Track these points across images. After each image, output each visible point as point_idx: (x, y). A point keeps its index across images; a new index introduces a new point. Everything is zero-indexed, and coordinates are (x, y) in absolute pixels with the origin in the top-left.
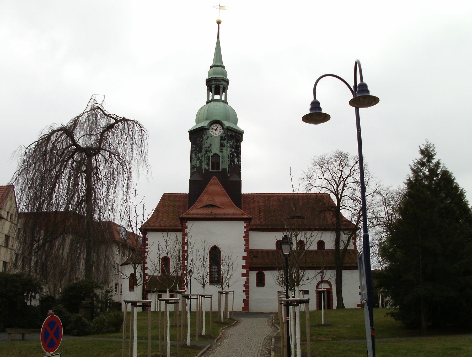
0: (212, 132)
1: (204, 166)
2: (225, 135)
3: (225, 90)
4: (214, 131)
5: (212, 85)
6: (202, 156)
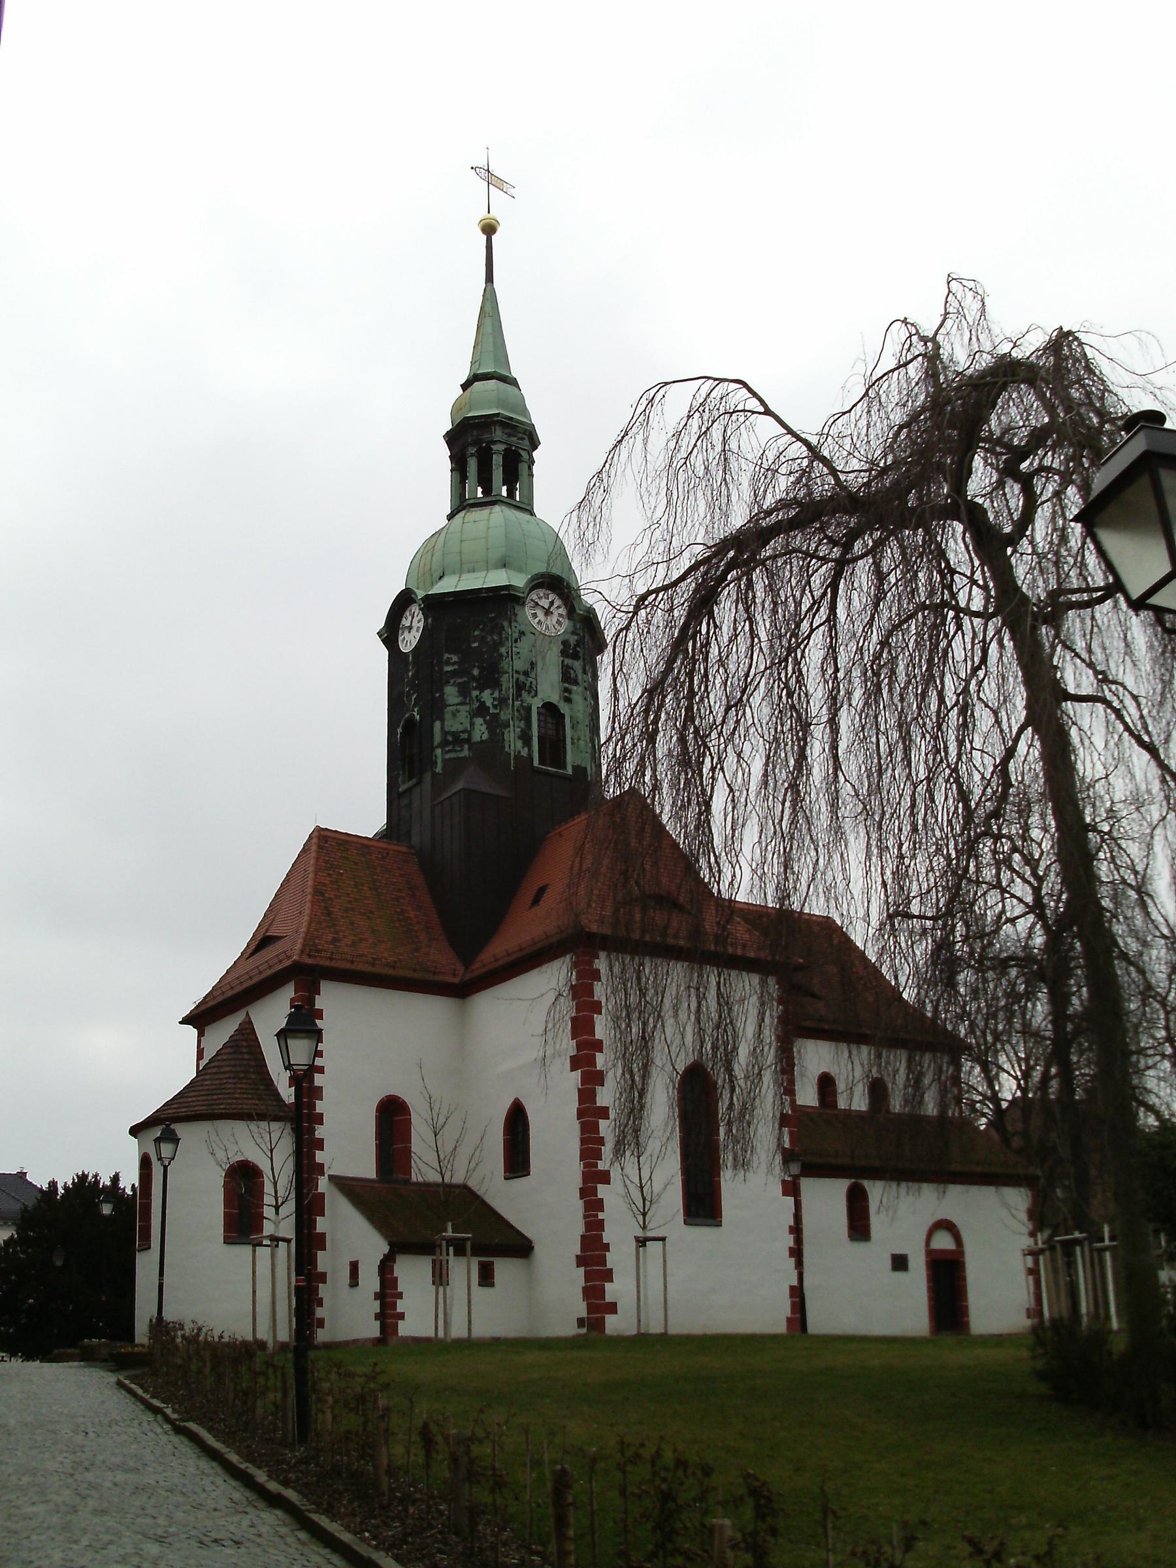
0: (535, 616)
1: (513, 743)
4: (541, 615)
5: (495, 442)
6: (502, 702)
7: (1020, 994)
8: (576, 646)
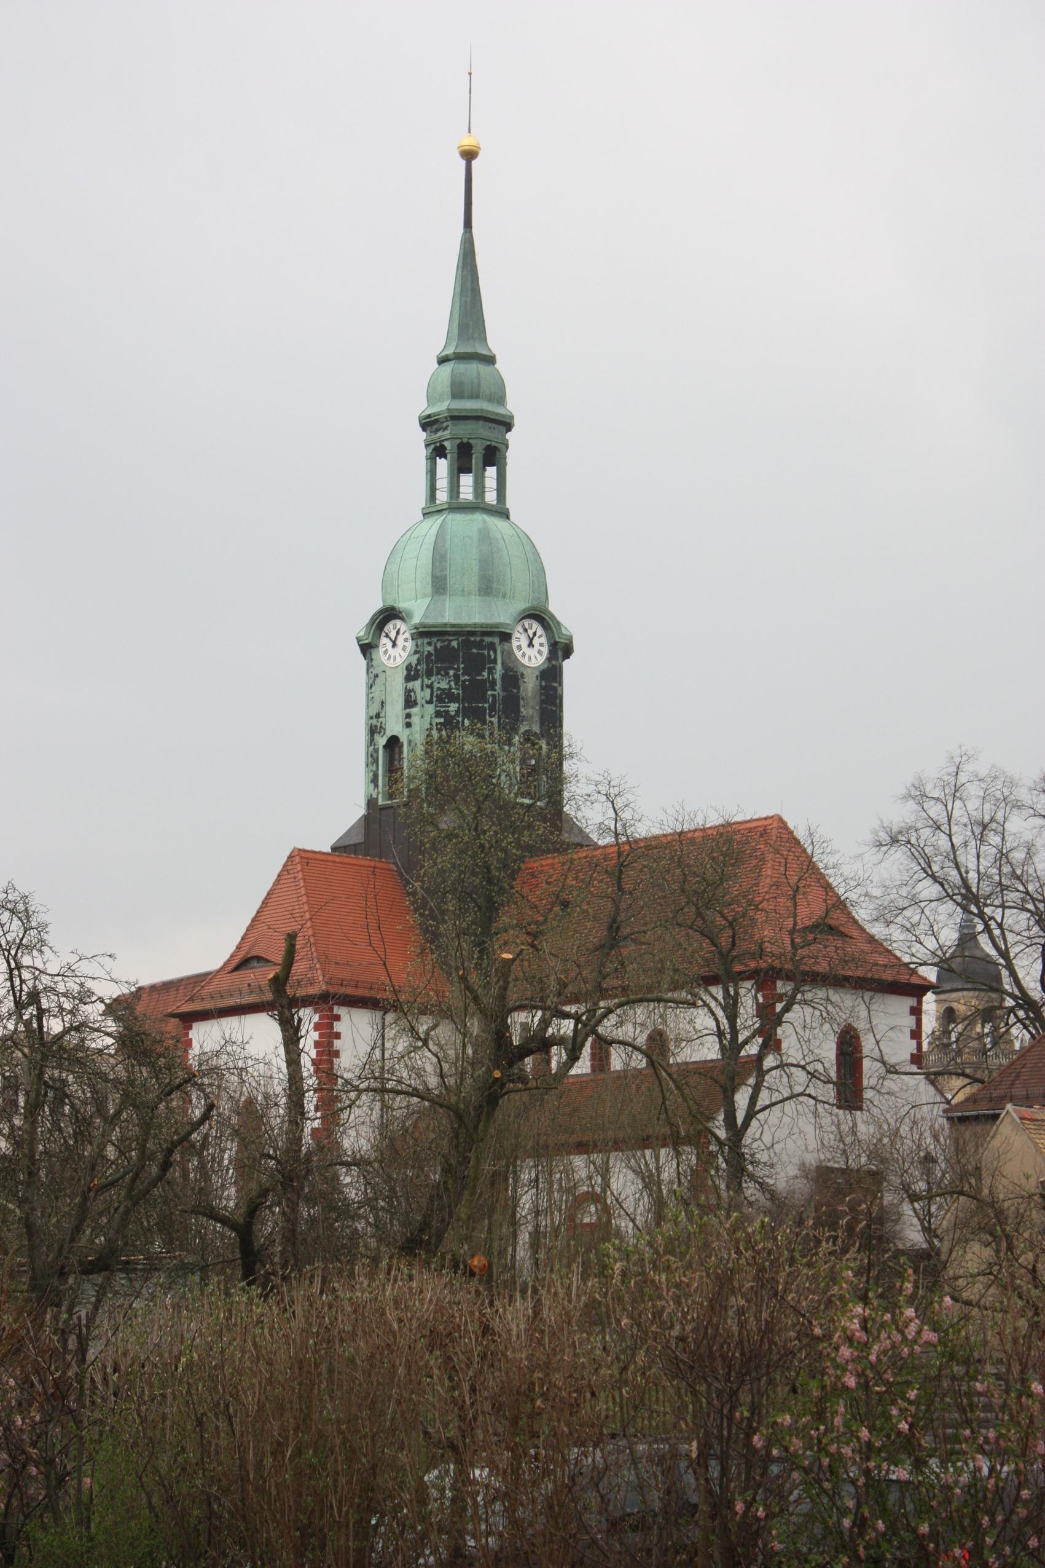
2: (417, 656)
3: (494, 456)
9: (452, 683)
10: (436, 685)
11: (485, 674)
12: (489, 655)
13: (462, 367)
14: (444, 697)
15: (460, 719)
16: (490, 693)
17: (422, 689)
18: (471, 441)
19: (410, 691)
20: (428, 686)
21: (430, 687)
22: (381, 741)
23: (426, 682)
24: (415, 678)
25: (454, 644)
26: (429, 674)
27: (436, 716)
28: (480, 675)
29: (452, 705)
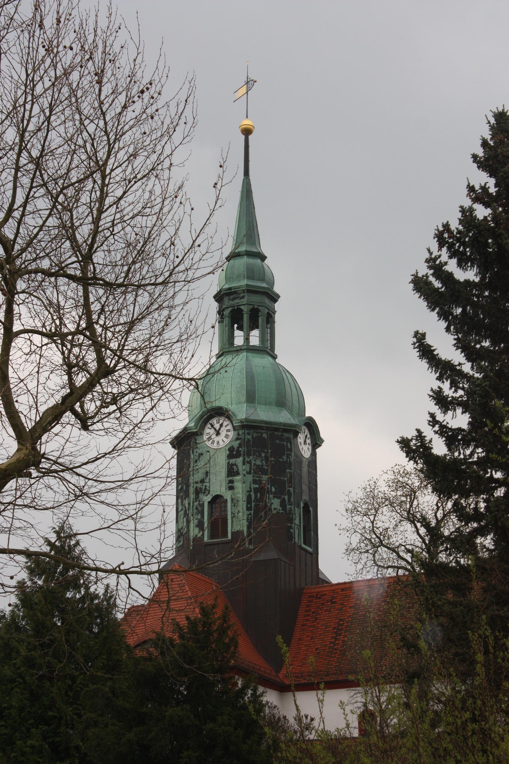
2: (239, 442)
7: (442, 536)
8: (238, 448)
9: (264, 462)
10: (253, 462)
11: (285, 457)
12: (287, 446)
13: (252, 261)
14: (260, 470)
15: (269, 487)
16: (288, 470)
17: (244, 464)
18: (260, 308)
19: (232, 465)
20: (248, 462)
21: (250, 462)
22: (206, 499)
23: (247, 459)
24: (238, 456)
25: (265, 435)
26: (249, 455)
27: (254, 483)
28: (282, 458)
29: (264, 476)
